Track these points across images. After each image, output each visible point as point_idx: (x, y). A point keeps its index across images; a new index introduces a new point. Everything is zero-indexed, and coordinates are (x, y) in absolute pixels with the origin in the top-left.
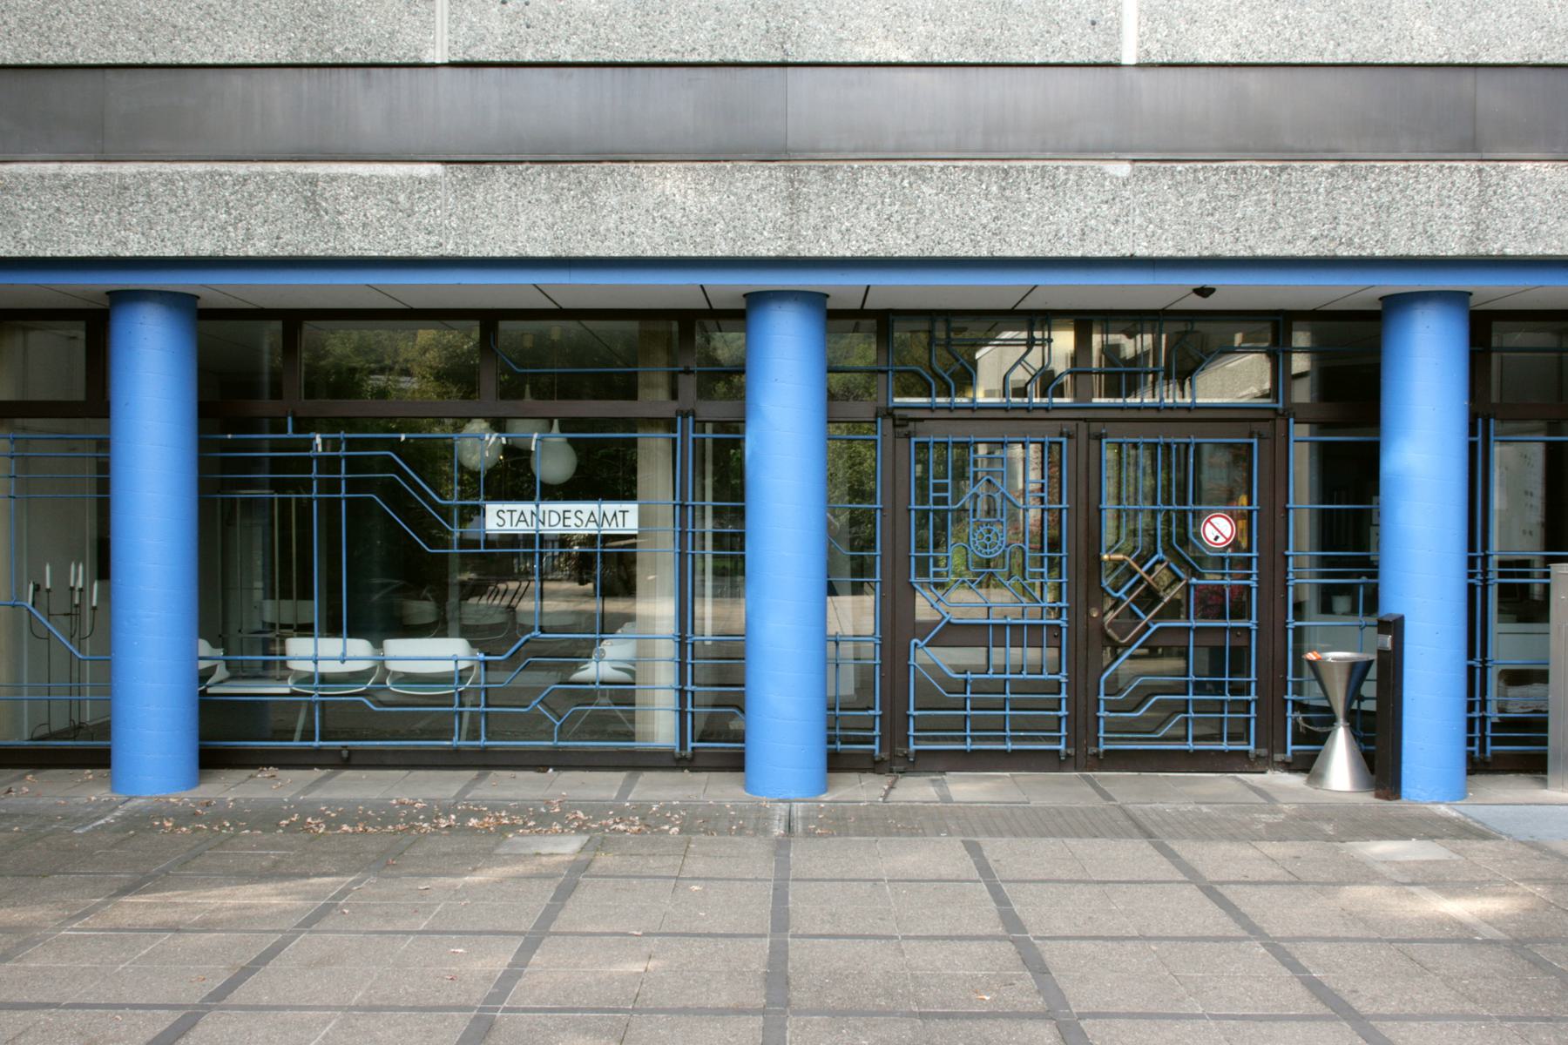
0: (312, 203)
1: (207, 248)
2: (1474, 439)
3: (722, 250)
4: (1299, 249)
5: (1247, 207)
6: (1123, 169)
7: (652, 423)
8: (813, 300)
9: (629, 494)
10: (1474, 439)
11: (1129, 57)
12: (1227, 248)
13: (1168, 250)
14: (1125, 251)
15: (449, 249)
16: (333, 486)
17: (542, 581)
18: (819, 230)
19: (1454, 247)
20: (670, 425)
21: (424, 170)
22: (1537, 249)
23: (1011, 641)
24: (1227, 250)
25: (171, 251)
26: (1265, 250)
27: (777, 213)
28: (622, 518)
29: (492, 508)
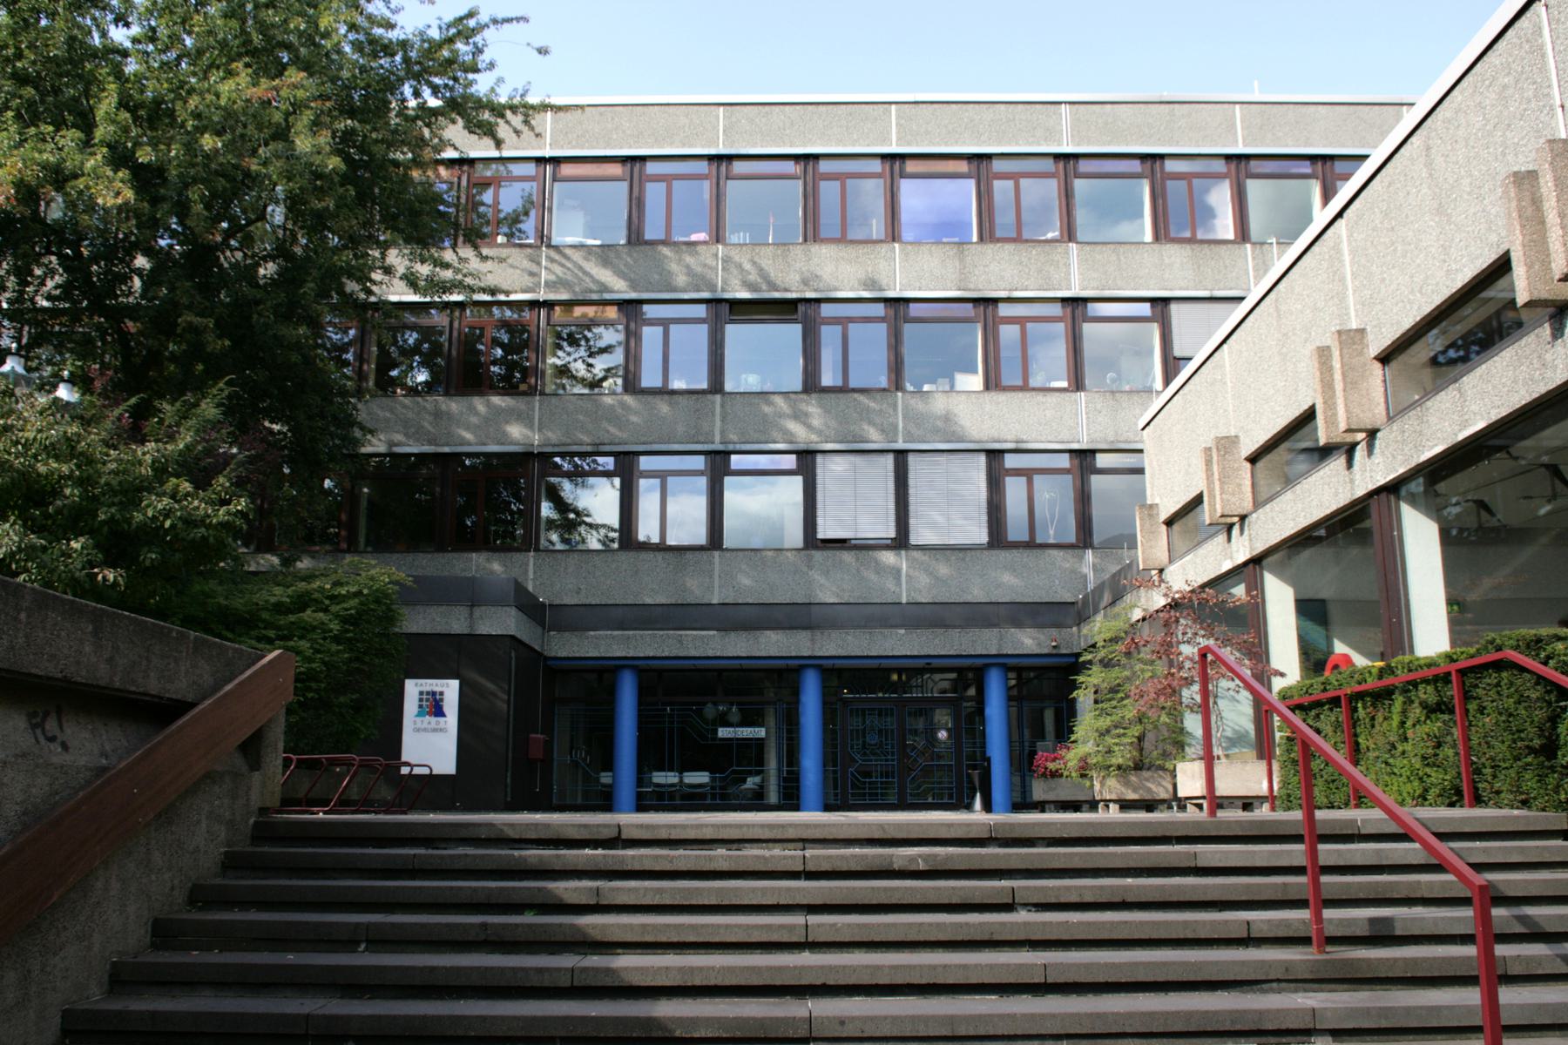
0: (680, 642)
1: (651, 654)
2: (678, 797)
3: (794, 654)
4: (951, 653)
5: (937, 641)
6: (903, 631)
7: (769, 703)
8: (819, 668)
9: (761, 725)
10: (678, 797)
11: (904, 601)
12: (932, 653)
13: (916, 653)
14: (904, 653)
15: (718, 654)
16: (673, 723)
17: (1209, 760)
18: (820, 649)
19: (994, 652)
20: (775, 703)
21: (712, 633)
22: (1017, 652)
23: (831, 757)
24: (932, 653)
25: (642, 655)
26: (943, 653)
27: (809, 644)
28: (761, 732)
29: (720, 730)
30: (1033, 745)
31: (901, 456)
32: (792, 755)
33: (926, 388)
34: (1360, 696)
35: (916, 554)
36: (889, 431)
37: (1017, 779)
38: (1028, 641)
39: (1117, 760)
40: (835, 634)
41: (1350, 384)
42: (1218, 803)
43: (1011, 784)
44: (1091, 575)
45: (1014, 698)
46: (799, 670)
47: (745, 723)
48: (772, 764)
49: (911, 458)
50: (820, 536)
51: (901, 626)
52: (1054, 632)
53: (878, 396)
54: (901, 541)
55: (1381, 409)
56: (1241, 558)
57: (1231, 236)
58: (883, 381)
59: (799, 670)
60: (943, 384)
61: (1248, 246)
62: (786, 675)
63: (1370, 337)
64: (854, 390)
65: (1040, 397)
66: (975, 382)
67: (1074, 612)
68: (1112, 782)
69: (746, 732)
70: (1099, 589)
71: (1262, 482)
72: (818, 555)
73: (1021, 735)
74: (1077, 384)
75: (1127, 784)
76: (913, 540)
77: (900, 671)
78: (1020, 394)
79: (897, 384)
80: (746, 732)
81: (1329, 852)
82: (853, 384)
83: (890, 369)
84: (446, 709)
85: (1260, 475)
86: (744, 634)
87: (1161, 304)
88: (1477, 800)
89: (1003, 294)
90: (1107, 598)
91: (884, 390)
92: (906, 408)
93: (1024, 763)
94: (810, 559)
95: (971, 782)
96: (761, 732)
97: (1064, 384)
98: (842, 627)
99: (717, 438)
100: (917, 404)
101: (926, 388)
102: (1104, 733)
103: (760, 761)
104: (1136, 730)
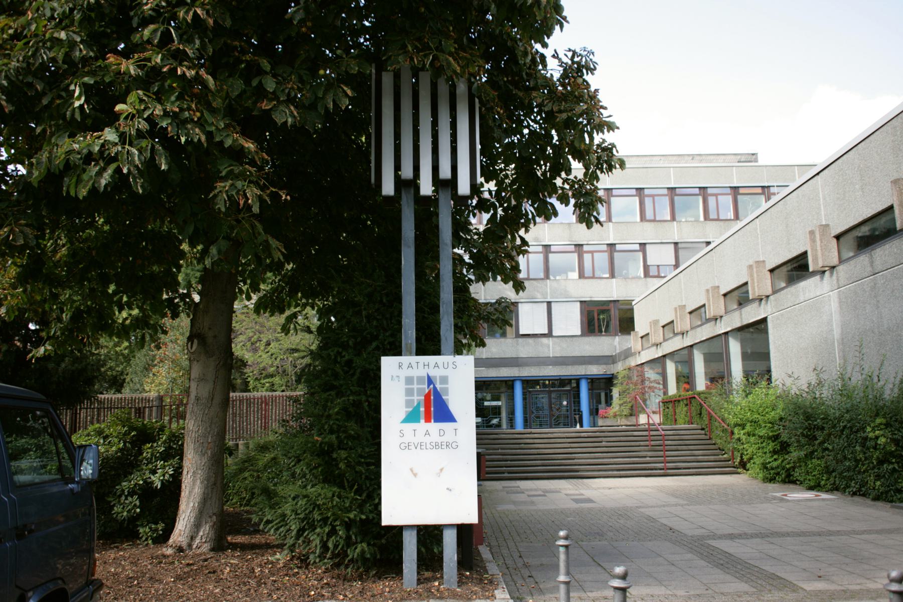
28: (499, 403)
30: (597, 406)
31: (549, 303)
32: (511, 413)
33: (558, 278)
34: (675, 401)
35: (555, 339)
36: (545, 295)
37: (592, 419)
38: (595, 370)
39: (625, 413)
40: (527, 368)
41: (681, 319)
42: (649, 424)
43: (590, 420)
44: (618, 347)
45: (591, 389)
46: (513, 381)
47: (493, 399)
48: (504, 414)
49: (553, 304)
50: (521, 333)
51: (550, 365)
52: (604, 366)
53: (540, 281)
54: (549, 334)
55: (689, 326)
56: (660, 355)
57: (669, 218)
58: (542, 275)
59: (513, 381)
60: (564, 277)
61: (675, 222)
62: (509, 384)
63: (687, 307)
64: (532, 279)
65: (599, 281)
66: (575, 275)
67: (611, 359)
68: (623, 420)
69: (494, 403)
70: (620, 354)
71: (666, 334)
72: (520, 340)
73: (593, 402)
74: (613, 276)
75: (628, 420)
76: (554, 334)
77: (549, 380)
78: (592, 280)
79: (547, 277)
80: (494, 403)
81: (652, 433)
82: (531, 277)
83: (544, 271)
84: (454, 407)
85: (665, 331)
86: (494, 369)
87: (643, 245)
88: (692, 424)
89: (585, 243)
90: (623, 357)
91: (542, 279)
92: (550, 286)
93: (594, 412)
94: (517, 341)
95: (575, 420)
96: (499, 403)
97: (608, 276)
98: (528, 366)
99: (483, 298)
100: (555, 284)
101: (558, 278)
102: (621, 405)
103: (500, 414)
104: (630, 405)
